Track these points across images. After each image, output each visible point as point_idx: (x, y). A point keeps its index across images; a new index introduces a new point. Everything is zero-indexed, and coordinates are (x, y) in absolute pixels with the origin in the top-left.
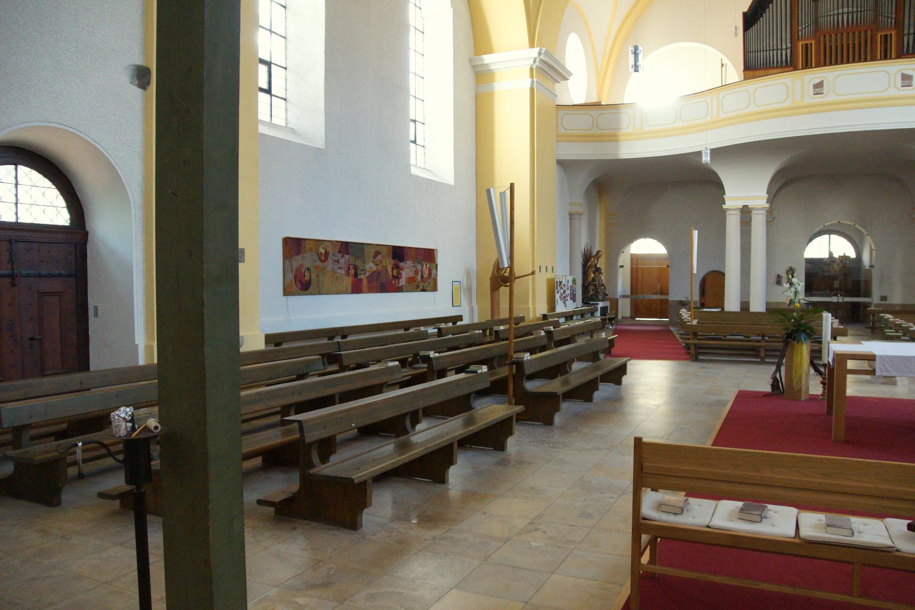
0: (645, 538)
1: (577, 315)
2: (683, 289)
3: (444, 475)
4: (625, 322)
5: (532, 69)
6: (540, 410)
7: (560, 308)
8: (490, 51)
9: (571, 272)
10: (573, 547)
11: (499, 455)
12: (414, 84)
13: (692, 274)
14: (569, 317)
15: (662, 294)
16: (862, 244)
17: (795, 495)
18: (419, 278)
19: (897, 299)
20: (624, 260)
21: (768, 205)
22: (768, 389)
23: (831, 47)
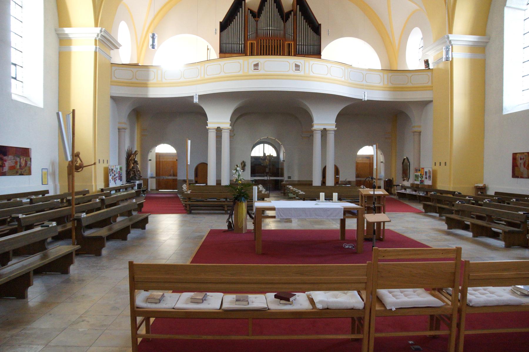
0: (139, 319)
1: (123, 189)
2: (186, 173)
3: (24, 293)
4: (153, 192)
5: (96, 40)
6: (91, 248)
7: (112, 185)
8: (69, 25)
9: (119, 164)
10: (105, 328)
11: (65, 277)
12: (14, 40)
13: (187, 164)
14: (117, 190)
15: (174, 176)
17: (223, 286)
18: (18, 167)
19: (296, 178)
20: (152, 156)
21: (230, 127)
22: (226, 228)
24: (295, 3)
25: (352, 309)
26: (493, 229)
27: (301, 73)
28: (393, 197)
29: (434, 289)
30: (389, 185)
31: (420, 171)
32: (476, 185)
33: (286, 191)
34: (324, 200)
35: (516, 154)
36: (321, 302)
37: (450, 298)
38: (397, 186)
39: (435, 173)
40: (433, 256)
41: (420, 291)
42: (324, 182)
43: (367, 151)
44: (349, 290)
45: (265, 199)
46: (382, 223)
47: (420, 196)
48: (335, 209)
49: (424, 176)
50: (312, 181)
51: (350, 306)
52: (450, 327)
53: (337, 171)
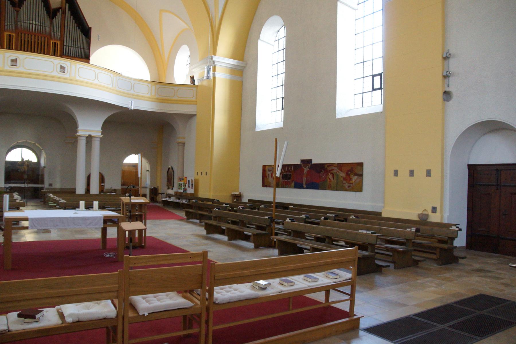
16: (40, 155)
19: (58, 185)
25: (105, 319)
26: (245, 232)
27: (66, 75)
28: (158, 204)
29: (186, 291)
30: (154, 192)
31: (183, 179)
32: (233, 193)
33: (46, 199)
34: (84, 209)
36: (71, 315)
38: (161, 194)
39: (197, 182)
40: (189, 260)
41: (172, 294)
42: (88, 190)
43: (133, 159)
44: (101, 300)
45: (21, 208)
46: (137, 232)
47: (183, 204)
49: (187, 185)
50: (75, 189)
51: (101, 316)
52: (200, 325)
53: (102, 179)
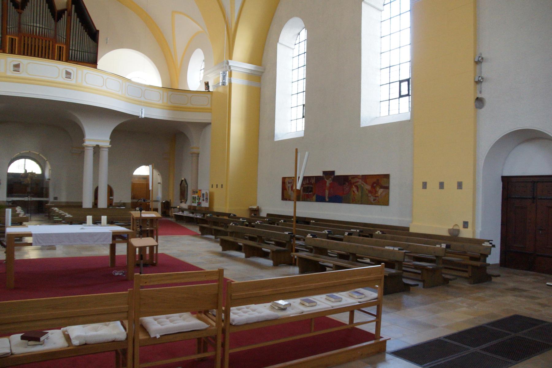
19: (63, 199)
21: (110, 146)
23: (28, 44)
24: (70, 3)
25: (114, 341)
26: (263, 249)
27: (72, 81)
28: (170, 219)
29: (200, 312)
30: (166, 206)
31: (197, 192)
32: (250, 207)
33: (51, 214)
34: (91, 224)
35: (285, 178)
36: (77, 337)
37: (214, 318)
38: (174, 208)
41: (186, 315)
42: (95, 204)
43: (143, 171)
45: (24, 223)
46: (148, 249)
47: (197, 218)
48: (104, 234)
50: (82, 203)
51: (111, 338)
53: (110, 192)
